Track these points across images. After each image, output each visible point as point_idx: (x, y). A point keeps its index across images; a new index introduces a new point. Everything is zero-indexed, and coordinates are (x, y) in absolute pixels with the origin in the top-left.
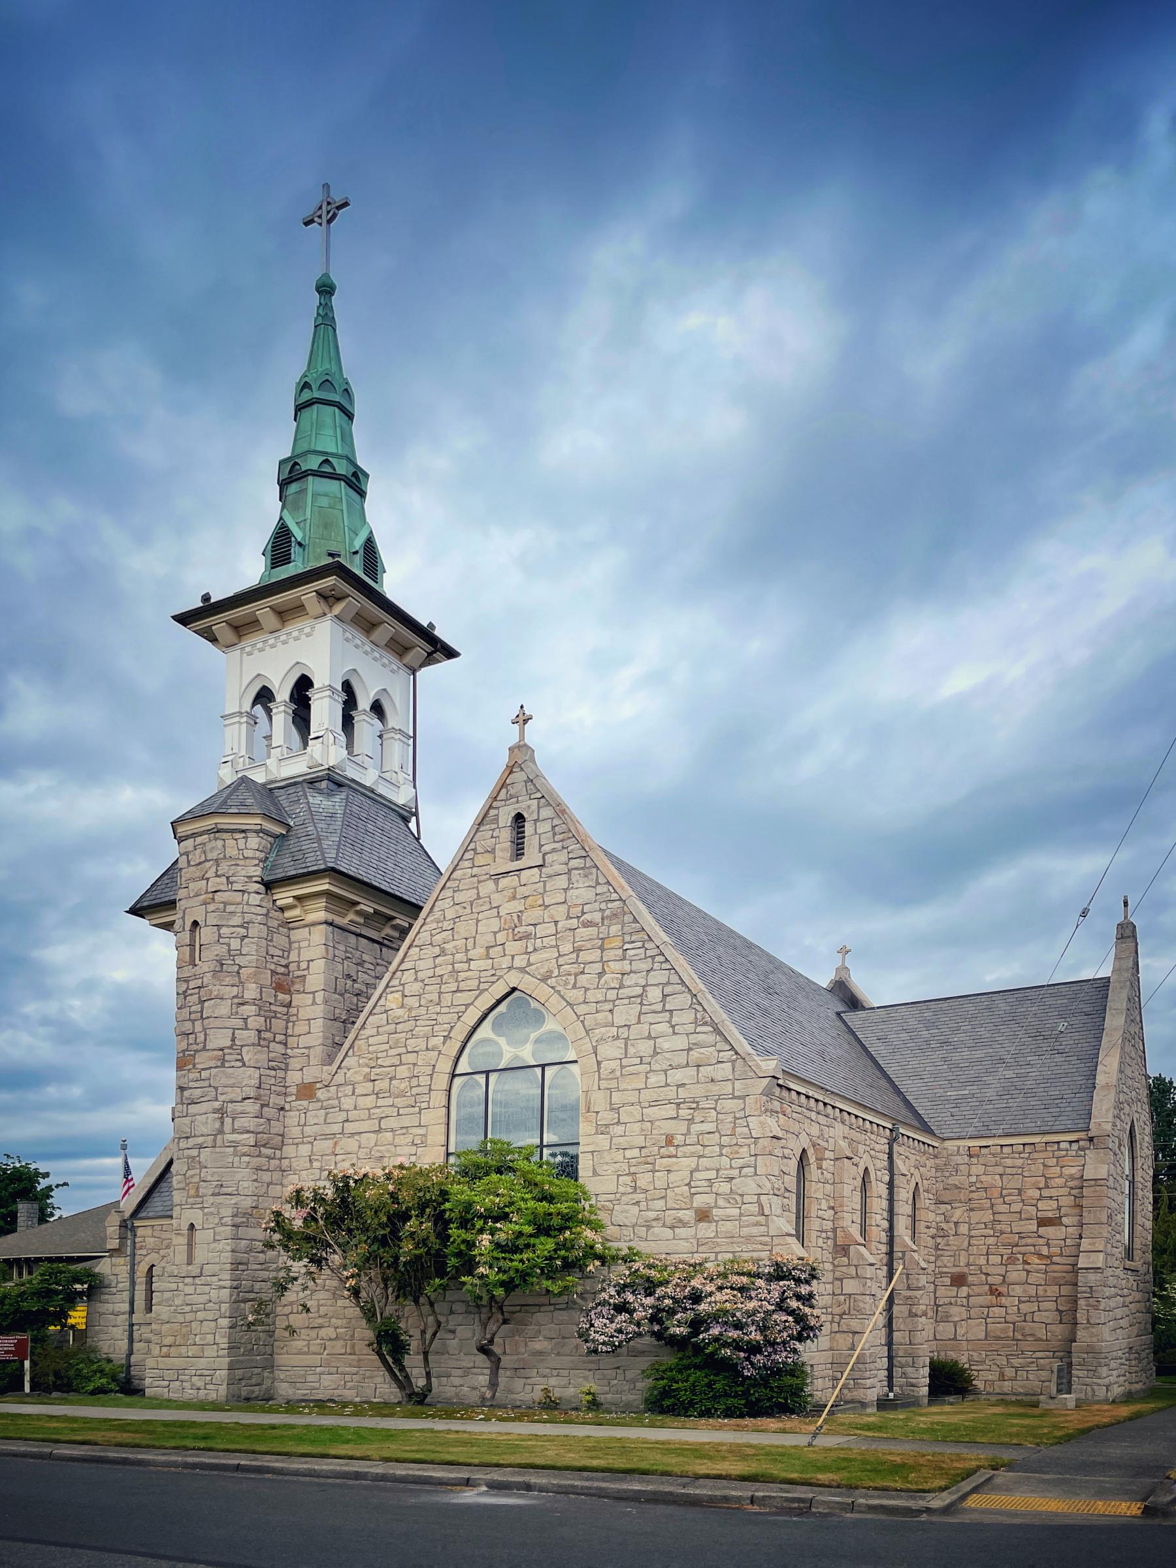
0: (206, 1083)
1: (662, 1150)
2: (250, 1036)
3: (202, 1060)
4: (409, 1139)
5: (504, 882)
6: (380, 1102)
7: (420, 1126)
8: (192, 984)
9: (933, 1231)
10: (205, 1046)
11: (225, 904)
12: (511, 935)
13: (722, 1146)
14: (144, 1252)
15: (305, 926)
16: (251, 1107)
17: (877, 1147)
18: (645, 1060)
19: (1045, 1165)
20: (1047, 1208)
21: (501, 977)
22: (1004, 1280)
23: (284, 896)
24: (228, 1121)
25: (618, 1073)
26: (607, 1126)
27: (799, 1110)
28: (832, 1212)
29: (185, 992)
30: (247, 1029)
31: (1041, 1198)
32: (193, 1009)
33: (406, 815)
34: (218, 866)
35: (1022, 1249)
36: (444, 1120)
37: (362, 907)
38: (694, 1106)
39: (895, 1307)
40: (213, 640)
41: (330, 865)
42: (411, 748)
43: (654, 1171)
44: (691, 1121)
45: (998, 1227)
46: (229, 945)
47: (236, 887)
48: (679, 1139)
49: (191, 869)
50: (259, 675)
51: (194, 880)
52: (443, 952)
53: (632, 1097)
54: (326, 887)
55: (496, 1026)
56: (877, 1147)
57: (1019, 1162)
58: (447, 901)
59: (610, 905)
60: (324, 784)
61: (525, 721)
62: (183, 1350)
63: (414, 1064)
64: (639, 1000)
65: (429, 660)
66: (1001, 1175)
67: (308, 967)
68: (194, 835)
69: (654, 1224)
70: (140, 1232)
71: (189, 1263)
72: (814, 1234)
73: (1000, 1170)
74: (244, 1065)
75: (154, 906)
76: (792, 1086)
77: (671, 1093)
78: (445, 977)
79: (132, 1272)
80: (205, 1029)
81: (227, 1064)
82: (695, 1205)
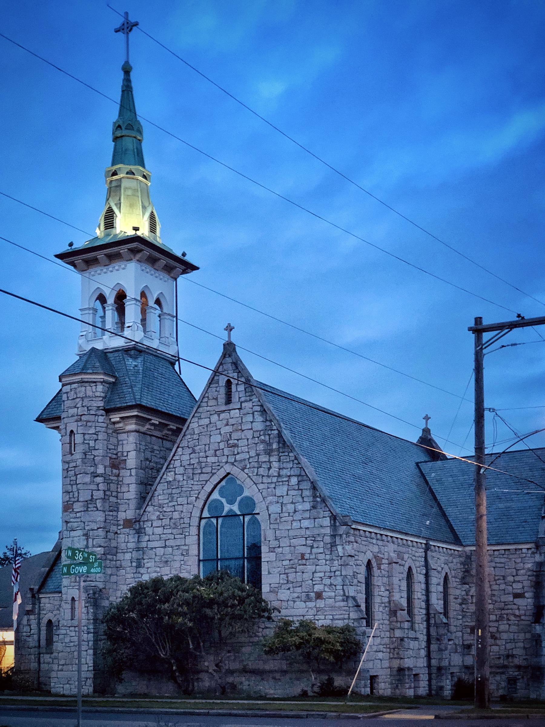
0: (79, 520)
1: (300, 561)
2: (100, 494)
3: (78, 507)
4: (180, 552)
5: (222, 416)
6: (165, 531)
7: (185, 545)
8: (72, 465)
9: (459, 601)
10: (78, 499)
11: (87, 421)
12: (226, 445)
13: (326, 560)
14: (44, 612)
15: (125, 433)
16: (101, 532)
17: (417, 554)
18: (291, 514)
19: (515, 562)
20: (517, 587)
21: (222, 467)
22: (497, 630)
23: (116, 417)
24: (90, 541)
25: (278, 521)
26: (274, 548)
27: (365, 539)
28: (388, 592)
29: (67, 469)
30: (99, 490)
31: (514, 581)
32: (72, 478)
33: (172, 361)
34: (83, 401)
35: (506, 612)
36: (197, 542)
37: (153, 421)
38: (313, 539)
39: (432, 646)
40: (75, 266)
41: (138, 403)
42: (175, 323)
43: (296, 572)
44: (312, 547)
45: (494, 598)
46: (89, 444)
47: (92, 412)
48: (307, 556)
49: (69, 402)
50: (98, 288)
51: (71, 408)
52: (194, 452)
53: (285, 534)
54: (136, 413)
55: (221, 494)
56: (417, 554)
57: (503, 560)
58: (195, 423)
59: (273, 432)
60: (132, 352)
61: (231, 330)
62: (70, 667)
63: (182, 511)
64: (287, 483)
65: (184, 272)
66: (494, 568)
67: (127, 456)
68: (70, 384)
69: (297, 600)
70: (43, 600)
71: (72, 619)
72: (377, 606)
73: (493, 564)
74: (97, 510)
75: (50, 417)
76: (359, 528)
77: (303, 532)
78: (196, 465)
79: (39, 624)
80: (78, 490)
81: (89, 509)
82: (315, 590)
